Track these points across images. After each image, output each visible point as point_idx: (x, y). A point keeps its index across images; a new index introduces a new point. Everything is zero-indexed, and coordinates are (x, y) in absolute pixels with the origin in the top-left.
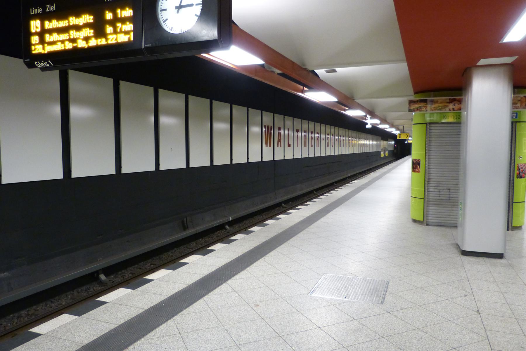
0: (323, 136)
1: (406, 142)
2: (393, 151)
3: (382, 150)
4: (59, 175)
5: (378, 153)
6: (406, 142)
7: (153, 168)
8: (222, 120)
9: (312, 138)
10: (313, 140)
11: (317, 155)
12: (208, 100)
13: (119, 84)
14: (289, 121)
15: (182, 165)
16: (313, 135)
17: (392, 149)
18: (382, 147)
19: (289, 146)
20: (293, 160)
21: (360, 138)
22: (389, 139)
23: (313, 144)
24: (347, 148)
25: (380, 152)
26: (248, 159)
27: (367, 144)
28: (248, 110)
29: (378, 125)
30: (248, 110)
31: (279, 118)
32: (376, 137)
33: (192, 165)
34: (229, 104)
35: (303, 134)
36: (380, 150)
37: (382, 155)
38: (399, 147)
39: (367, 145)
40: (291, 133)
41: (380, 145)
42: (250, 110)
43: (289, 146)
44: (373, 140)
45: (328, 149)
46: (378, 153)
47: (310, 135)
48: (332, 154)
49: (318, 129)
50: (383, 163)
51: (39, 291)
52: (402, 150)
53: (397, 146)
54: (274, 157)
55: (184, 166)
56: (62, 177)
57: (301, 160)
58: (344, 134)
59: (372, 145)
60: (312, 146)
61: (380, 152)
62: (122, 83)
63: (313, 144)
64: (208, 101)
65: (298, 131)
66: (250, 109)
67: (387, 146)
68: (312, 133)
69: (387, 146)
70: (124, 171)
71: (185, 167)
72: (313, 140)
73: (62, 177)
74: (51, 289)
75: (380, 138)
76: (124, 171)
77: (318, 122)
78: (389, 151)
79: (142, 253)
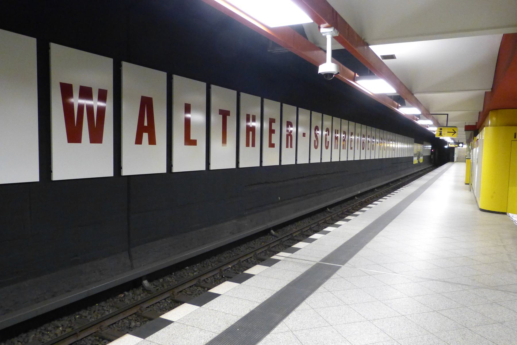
0: (377, 140)
1: (446, 147)
2: (429, 157)
3: (415, 155)
4: (110, 173)
5: (411, 159)
6: (446, 147)
7: (258, 165)
8: (198, 109)
9: (369, 142)
10: (353, 143)
11: (351, 159)
12: (235, 92)
13: (121, 66)
14: (304, 115)
15: (294, 163)
16: (353, 137)
17: (428, 154)
18: (415, 152)
19: (351, 148)
20: (297, 167)
21: (389, 140)
22: (425, 142)
23: (353, 146)
24: (357, 152)
25: (412, 158)
26: (296, 160)
27: (397, 147)
28: (322, 116)
29: (428, 127)
30: (282, 106)
31: (290, 110)
32: (406, 138)
33: (298, 163)
34: (204, 84)
35: (357, 137)
36: (412, 155)
37: (415, 161)
38: (437, 154)
39: (394, 149)
40: (359, 138)
41: (412, 149)
42: (342, 120)
43: (272, 145)
44: (408, 143)
45: (363, 152)
46: (411, 159)
47: (350, 137)
48: (373, 158)
49: (358, 130)
50: (416, 171)
51: (30, 317)
52: (441, 156)
53: (435, 151)
54: (310, 159)
55: (258, 165)
56: (38, 180)
57: (340, 163)
58: (385, 136)
59: (402, 149)
60: (272, 145)
61: (412, 158)
62: (125, 64)
63: (353, 146)
64: (163, 75)
65: (317, 128)
66: (324, 115)
67: (421, 151)
68: (352, 134)
69: (421, 151)
70: (175, 169)
71: (165, 171)
72: (353, 143)
73: (38, 180)
74: (229, 244)
75: (413, 140)
76: (175, 169)
77: (353, 121)
78: (424, 157)
79: (30, 317)
